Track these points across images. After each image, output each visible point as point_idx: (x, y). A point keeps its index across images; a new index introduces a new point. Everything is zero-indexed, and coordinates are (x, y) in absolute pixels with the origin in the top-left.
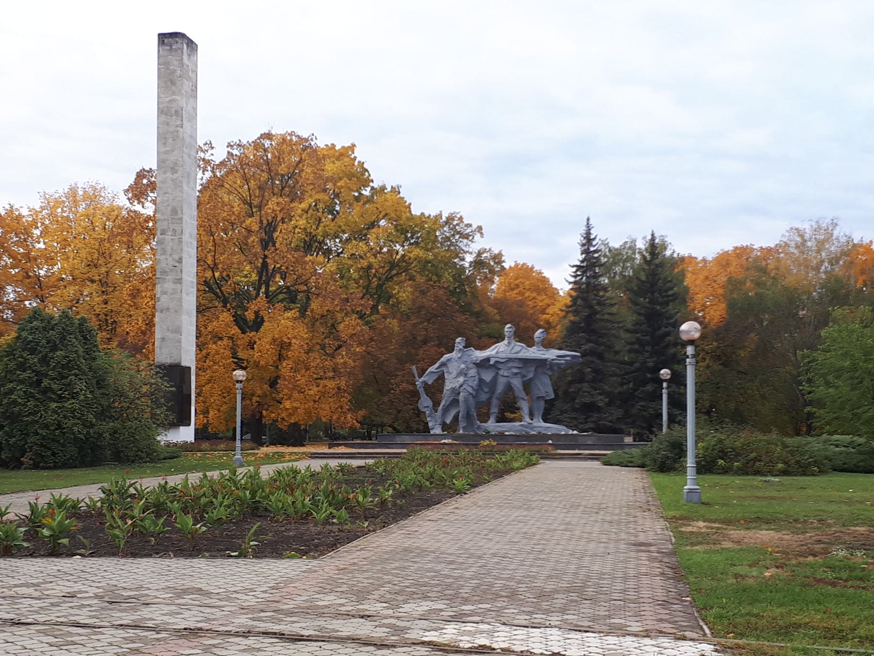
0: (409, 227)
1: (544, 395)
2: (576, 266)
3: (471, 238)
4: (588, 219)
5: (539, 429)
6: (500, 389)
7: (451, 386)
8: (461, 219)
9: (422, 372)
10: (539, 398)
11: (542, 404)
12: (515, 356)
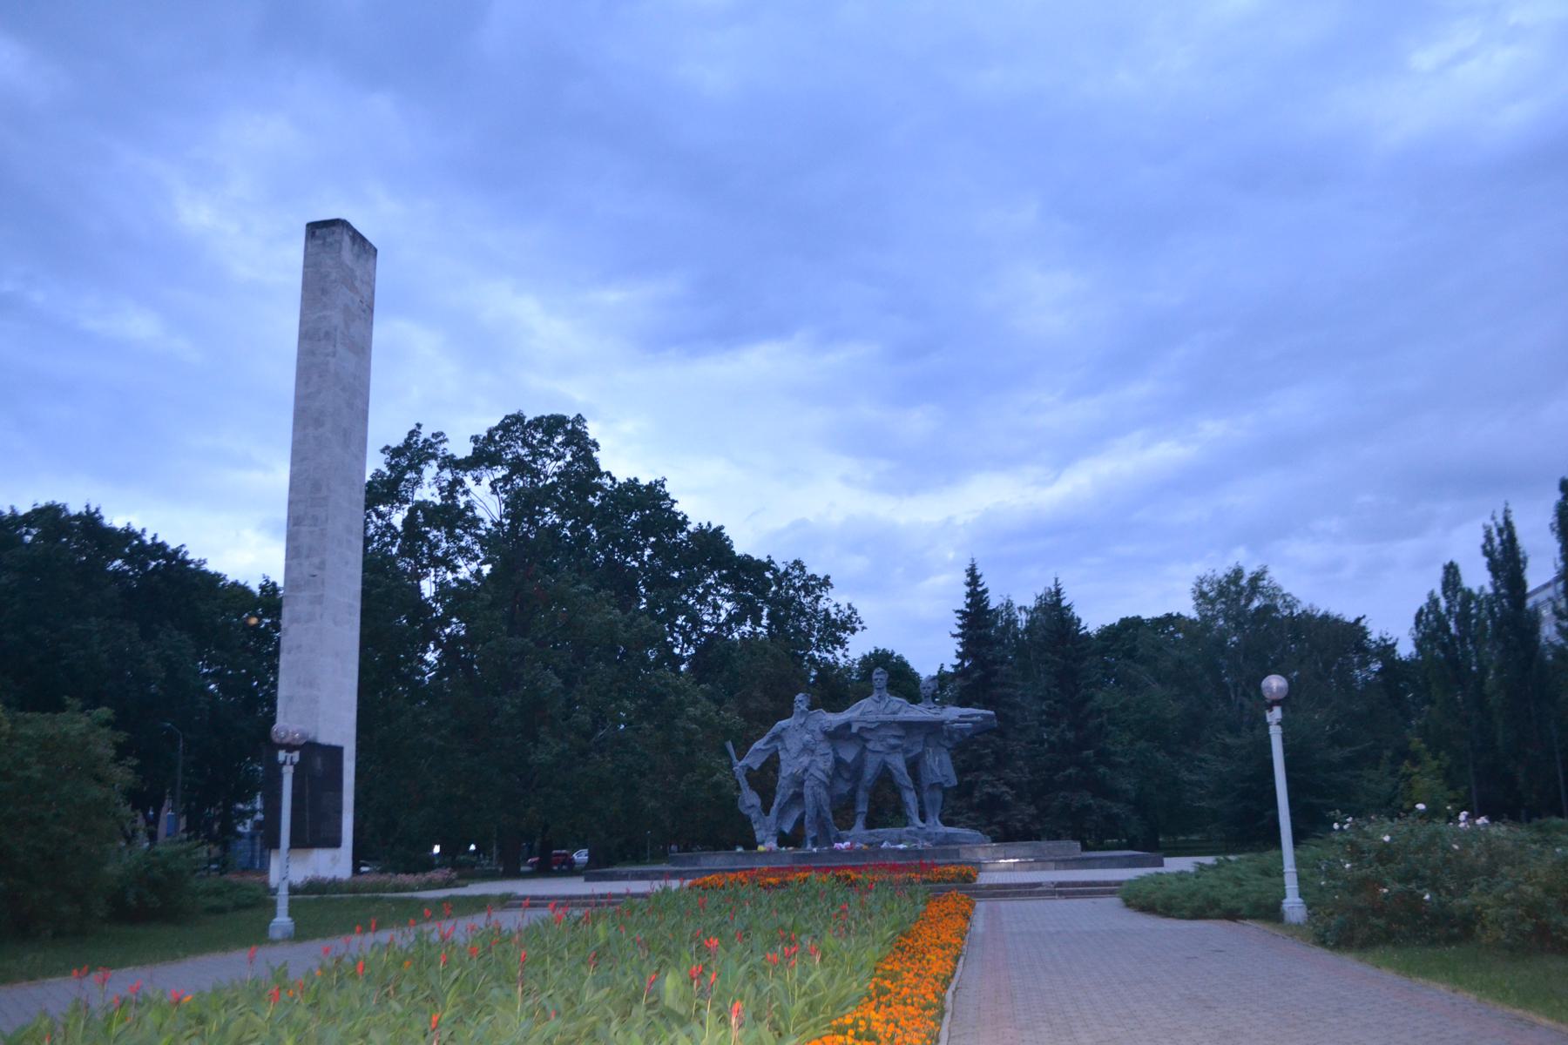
1: (942, 780)
6: (870, 772)
7: (790, 770)
10: (932, 786)
11: (939, 795)
12: (891, 718)
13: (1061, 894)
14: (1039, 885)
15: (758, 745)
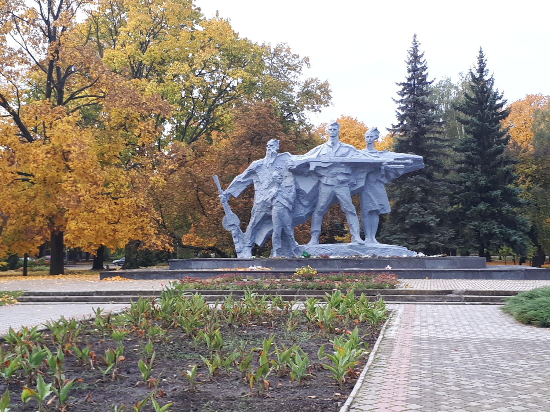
0: (237, 54)
1: (378, 208)
2: (404, 84)
3: (298, 69)
4: (415, 36)
5: (373, 251)
6: (323, 201)
7: (263, 198)
8: (288, 50)
9: (225, 183)
10: (371, 213)
11: (376, 220)
12: (340, 159)
13: (467, 300)
14: (450, 292)
15: (237, 178)
